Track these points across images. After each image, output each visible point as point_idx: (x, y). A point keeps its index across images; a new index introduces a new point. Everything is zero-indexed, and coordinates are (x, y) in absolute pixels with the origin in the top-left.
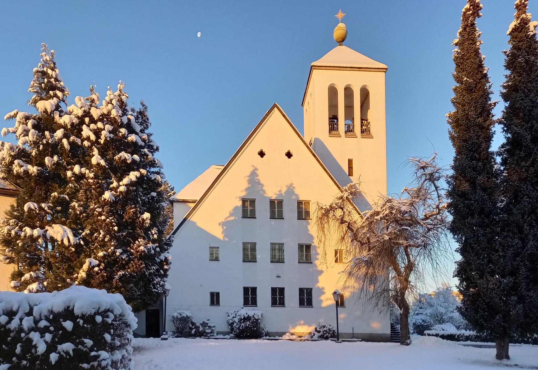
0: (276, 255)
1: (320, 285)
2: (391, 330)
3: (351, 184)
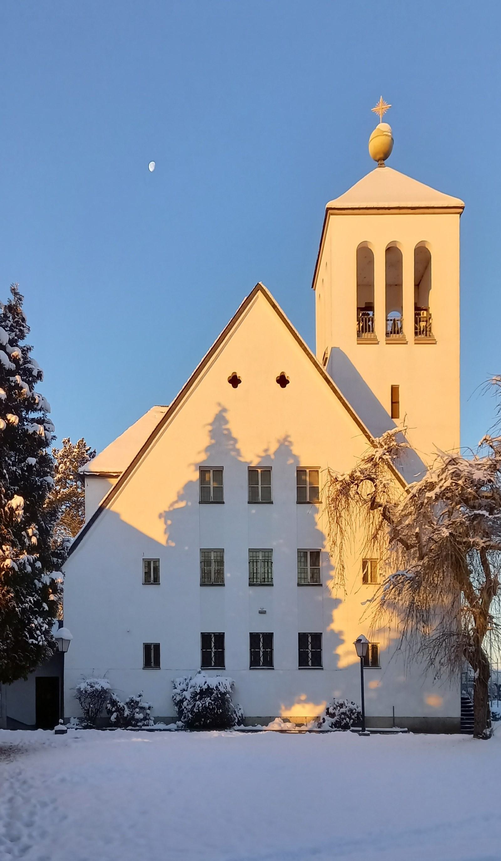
0: (259, 571)
1: (335, 626)
2: (462, 711)
3: (389, 431)
